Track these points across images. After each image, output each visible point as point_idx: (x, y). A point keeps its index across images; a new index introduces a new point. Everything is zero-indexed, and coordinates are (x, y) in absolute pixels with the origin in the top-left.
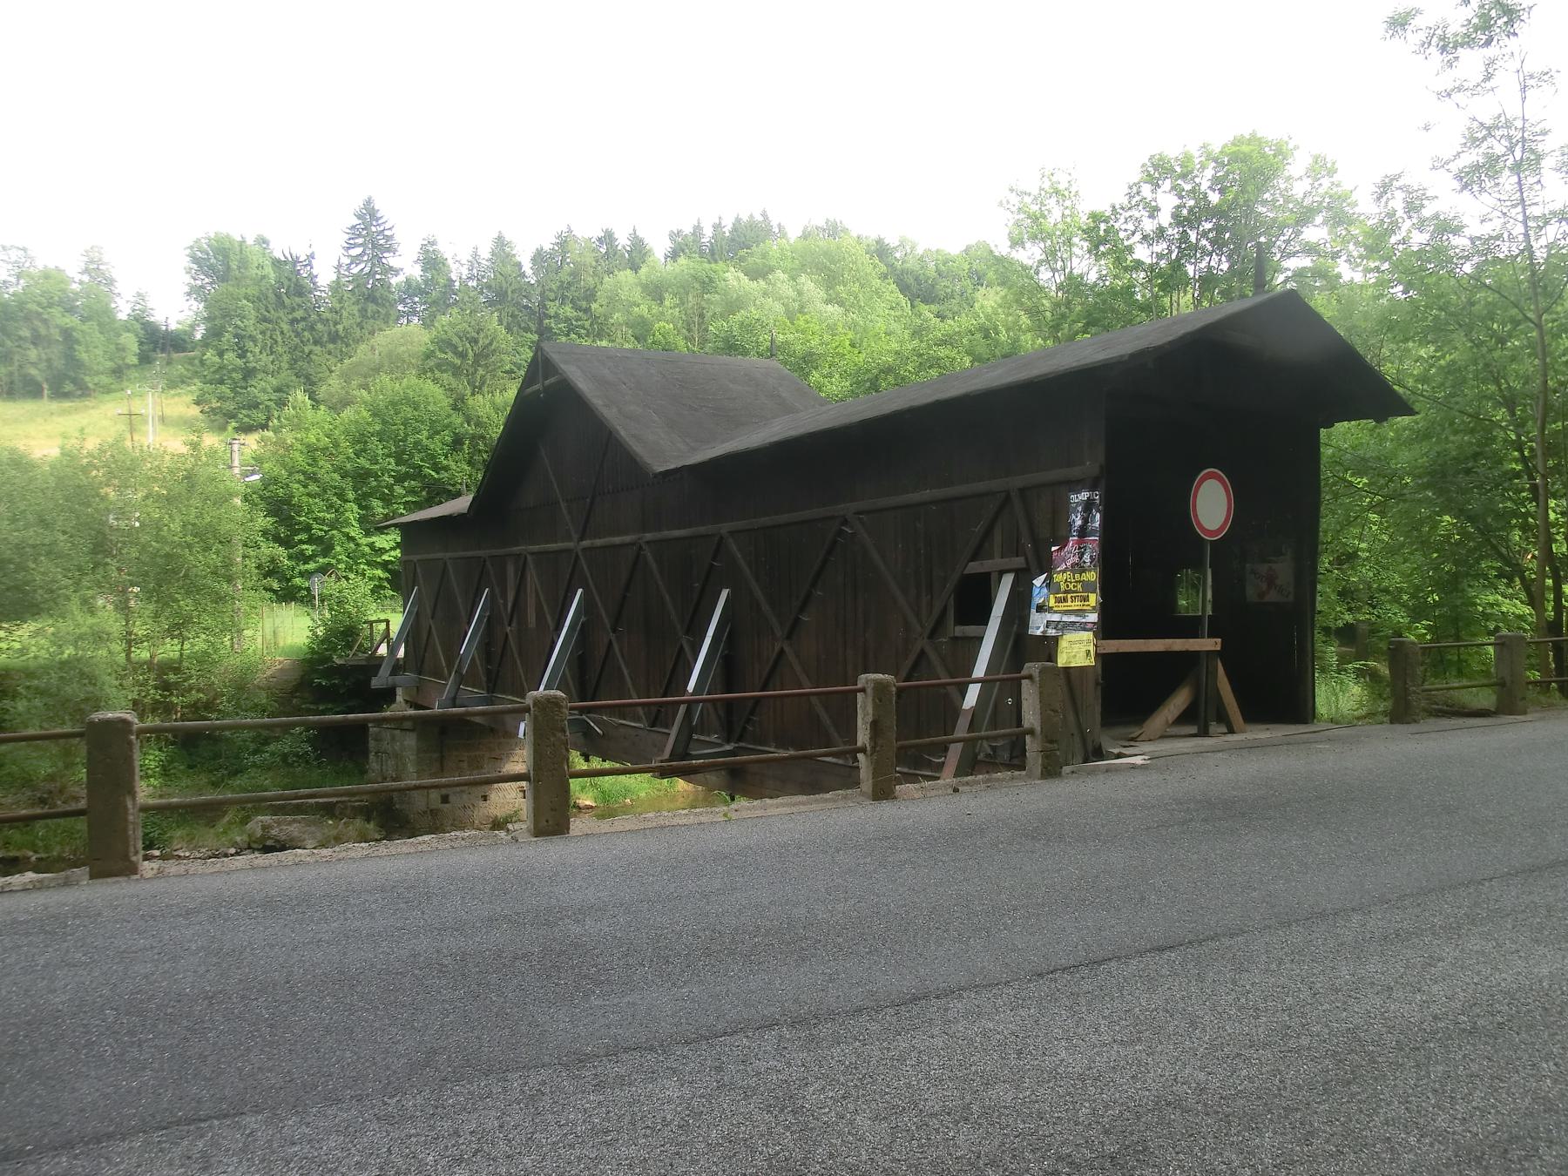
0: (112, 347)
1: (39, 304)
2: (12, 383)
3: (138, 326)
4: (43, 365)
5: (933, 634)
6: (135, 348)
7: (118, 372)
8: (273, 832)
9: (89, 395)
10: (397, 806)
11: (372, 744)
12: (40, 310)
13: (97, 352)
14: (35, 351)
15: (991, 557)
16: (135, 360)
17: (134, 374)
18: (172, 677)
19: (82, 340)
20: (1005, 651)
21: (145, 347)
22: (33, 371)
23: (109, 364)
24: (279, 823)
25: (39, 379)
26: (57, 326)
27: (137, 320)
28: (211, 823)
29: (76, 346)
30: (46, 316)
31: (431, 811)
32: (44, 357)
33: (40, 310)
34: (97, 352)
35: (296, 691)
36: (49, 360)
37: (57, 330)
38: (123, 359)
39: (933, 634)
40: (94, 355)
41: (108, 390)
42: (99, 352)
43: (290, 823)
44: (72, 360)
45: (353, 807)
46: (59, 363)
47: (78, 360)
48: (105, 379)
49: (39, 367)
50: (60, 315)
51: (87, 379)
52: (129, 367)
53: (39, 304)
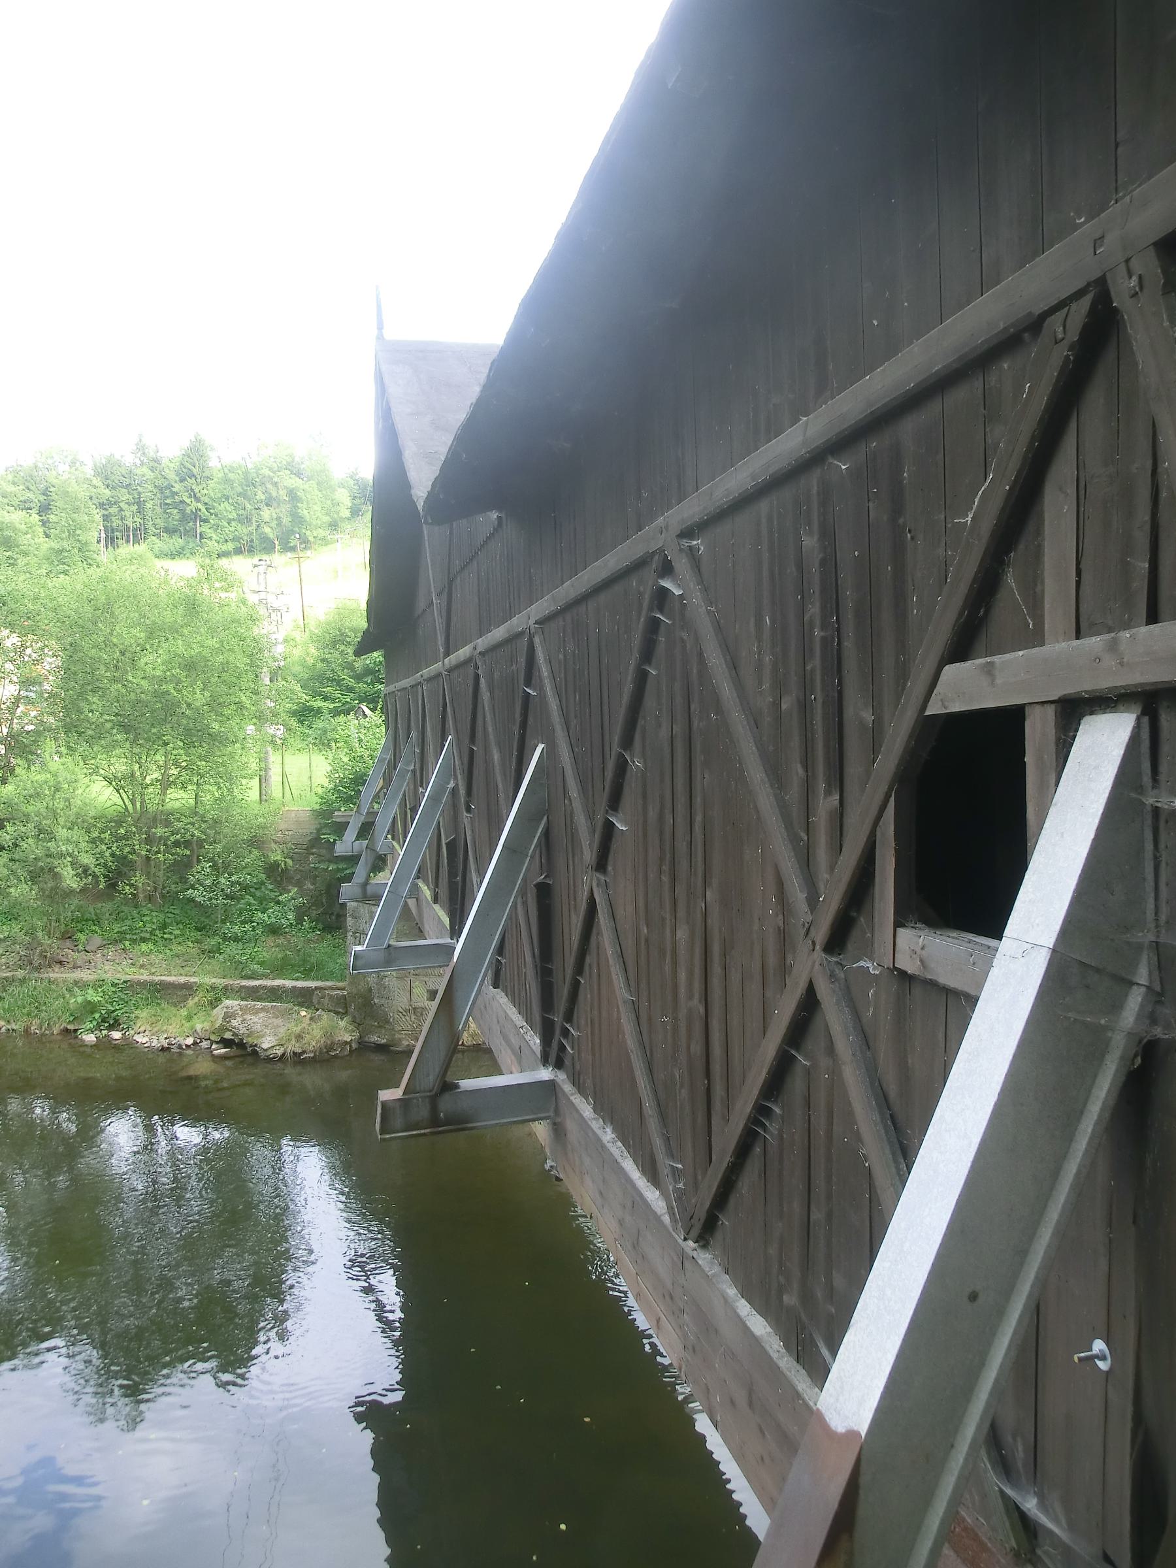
0: (329, 502)
1: (271, 469)
2: (252, 541)
3: (351, 482)
4: (274, 524)
5: (837, 941)
6: (348, 502)
7: (334, 526)
8: (234, 1023)
9: (310, 548)
10: (376, 1001)
11: (350, 921)
12: (272, 474)
13: (315, 507)
14: (268, 512)
15: (1036, 638)
16: (347, 514)
17: (347, 526)
18: (159, 831)
19: (304, 497)
20: (1069, 1138)
21: (358, 501)
22: (267, 530)
23: (327, 519)
24: (244, 1010)
25: (271, 536)
26: (285, 487)
27: (351, 477)
28: (181, 1002)
29: (299, 505)
30: (276, 479)
31: (415, 1009)
32: (275, 516)
33: (272, 474)
34: (315, 507)
35: (312, 847)
36: (278, 518)
37: (285, 491)
38: (338, 513)
39: (837, 941)
40: (314, 513)
41: (324, 542)
42: (317, 508)
43: (257, 1012)
44: (298, 520)
45: (331, 997)
46: (286, 520)
47: (301, 517)
48: (321, 533)
49: (271, 525)
50: (287, 478)
51: (308, 533)
52: (343, 520)
53: (271, 469)
